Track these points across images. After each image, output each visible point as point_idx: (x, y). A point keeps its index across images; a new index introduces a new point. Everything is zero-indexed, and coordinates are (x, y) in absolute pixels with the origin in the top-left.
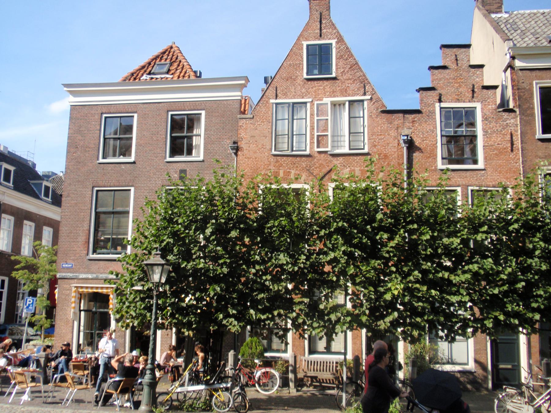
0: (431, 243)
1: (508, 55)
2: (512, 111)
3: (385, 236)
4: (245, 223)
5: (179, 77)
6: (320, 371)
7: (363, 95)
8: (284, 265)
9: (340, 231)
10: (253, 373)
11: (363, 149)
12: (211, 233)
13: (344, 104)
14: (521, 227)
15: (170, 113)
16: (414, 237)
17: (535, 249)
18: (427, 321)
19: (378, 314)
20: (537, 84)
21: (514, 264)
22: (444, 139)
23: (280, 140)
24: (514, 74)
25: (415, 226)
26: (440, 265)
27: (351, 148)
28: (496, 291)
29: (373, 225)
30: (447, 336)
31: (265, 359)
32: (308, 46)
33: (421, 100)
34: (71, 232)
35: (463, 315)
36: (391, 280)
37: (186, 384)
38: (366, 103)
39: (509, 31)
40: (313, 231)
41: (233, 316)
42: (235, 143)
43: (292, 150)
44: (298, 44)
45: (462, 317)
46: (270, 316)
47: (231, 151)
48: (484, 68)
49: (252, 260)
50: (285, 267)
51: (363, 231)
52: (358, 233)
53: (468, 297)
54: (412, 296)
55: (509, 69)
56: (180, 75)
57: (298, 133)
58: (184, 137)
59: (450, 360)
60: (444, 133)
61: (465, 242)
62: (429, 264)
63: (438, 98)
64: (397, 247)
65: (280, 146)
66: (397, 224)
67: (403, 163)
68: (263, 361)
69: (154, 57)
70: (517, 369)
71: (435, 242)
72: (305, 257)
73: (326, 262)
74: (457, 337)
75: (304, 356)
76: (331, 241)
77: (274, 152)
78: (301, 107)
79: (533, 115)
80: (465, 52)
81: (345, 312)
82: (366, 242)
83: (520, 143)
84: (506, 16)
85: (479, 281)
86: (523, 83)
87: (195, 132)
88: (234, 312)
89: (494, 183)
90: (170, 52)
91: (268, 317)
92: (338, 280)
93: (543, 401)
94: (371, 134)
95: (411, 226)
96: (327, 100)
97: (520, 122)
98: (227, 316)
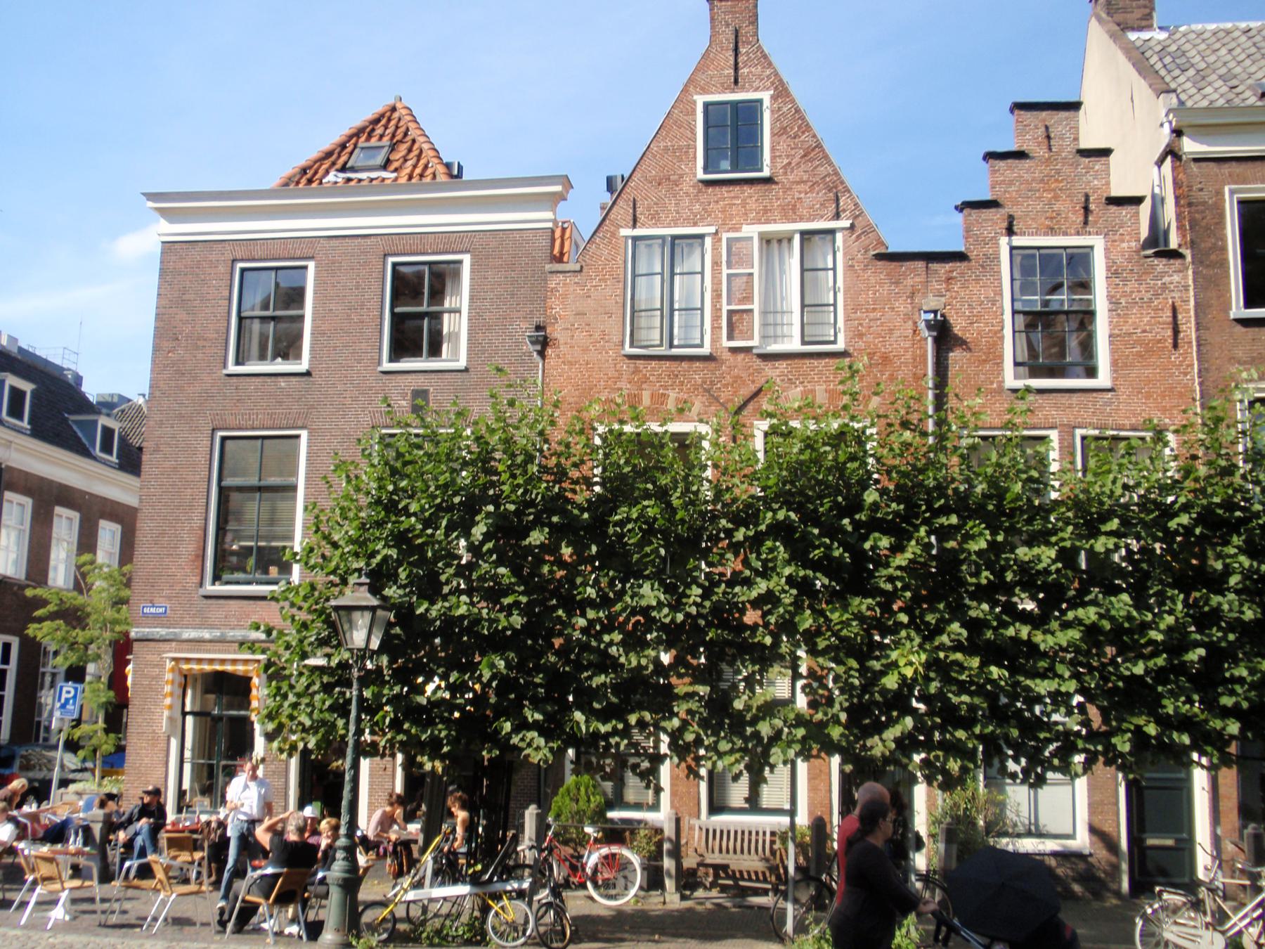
0: (989, 558)
1: (1167, 126)
2: (1175, 255)
3: (885, 542)
4: (564, 513)
5: (410, 177)
6: (735, 852)
7: (833, 219)
8: (653, 608)
9: (780, 530)
10: (582, 857)
11: (834, 342)
12: (484, 534)
13: (790, 240)
14: (1197, 522)
15: (391, 260)
16: (951, 544)
17: (1228, 571)
18: (981, 738)
19: (867, 721)
20: (1232, 192)
21: (1180, 606)
22: (1020, 319)
23: (643, 321)
24: (1181, 169)
25: (954, 519)
26: (1010, 609)
27: (806, 339)
28: (1139, 669)
29: (857, 517)
30: (1026, 771)
31: (608, 826)
32: (707, 106)
33: (968, 230)
34: (163, 534)
35: (1064, 724)
36: (897, 644)
37: (427, 881)
39: (1169, 72)
40: (719, 531)
41: (536, 726)
42: (539, 328)
43: (671, 346)
44: (683, 101)
45: (1060, 728)
47: (531, 348)
48: (1112, 157)
49: (578, 598)
50: (654, 614)
51: (833, 531)
52: (821, 535)
53: (1074, 681)
54: (947, 680)
55: (1169, 159)
56: (412, 171)
57: (683, 306)
58: (421, 316)
60: (1019, 306)
61: (1068, 557)
62: (985, 607)
63: (1005, 224)
64: (912, 568)
65: (642, 335)
66: (910, 514)
67: (925, 375)
68: (604, 830)
69: (354, 131)
70: (1186, 847)
71: (998, 557)
72: (700, 591)
73: (749, 601)
74: (1050, 775)
75: (699, 817)
76: (759, 554)
77: (628, 350)
78: (691, 245)
79: (1223, 264)
80: (1067, 118)
81: (792, 716)
82: (841, 555)
83: (1193, 330)
84: (1162, 36)
85: (1099, 646)
86: (1201, 190)
87: (447, 304)
88: (538, 716)
89: (1134, 421)
90: (389, 120)
91: (614, 728)
93: (1247, 920)
94: (852, 308)
95: (943, 520)
96: (752, 231)
97: (1194, 281)
98: (522, 725)
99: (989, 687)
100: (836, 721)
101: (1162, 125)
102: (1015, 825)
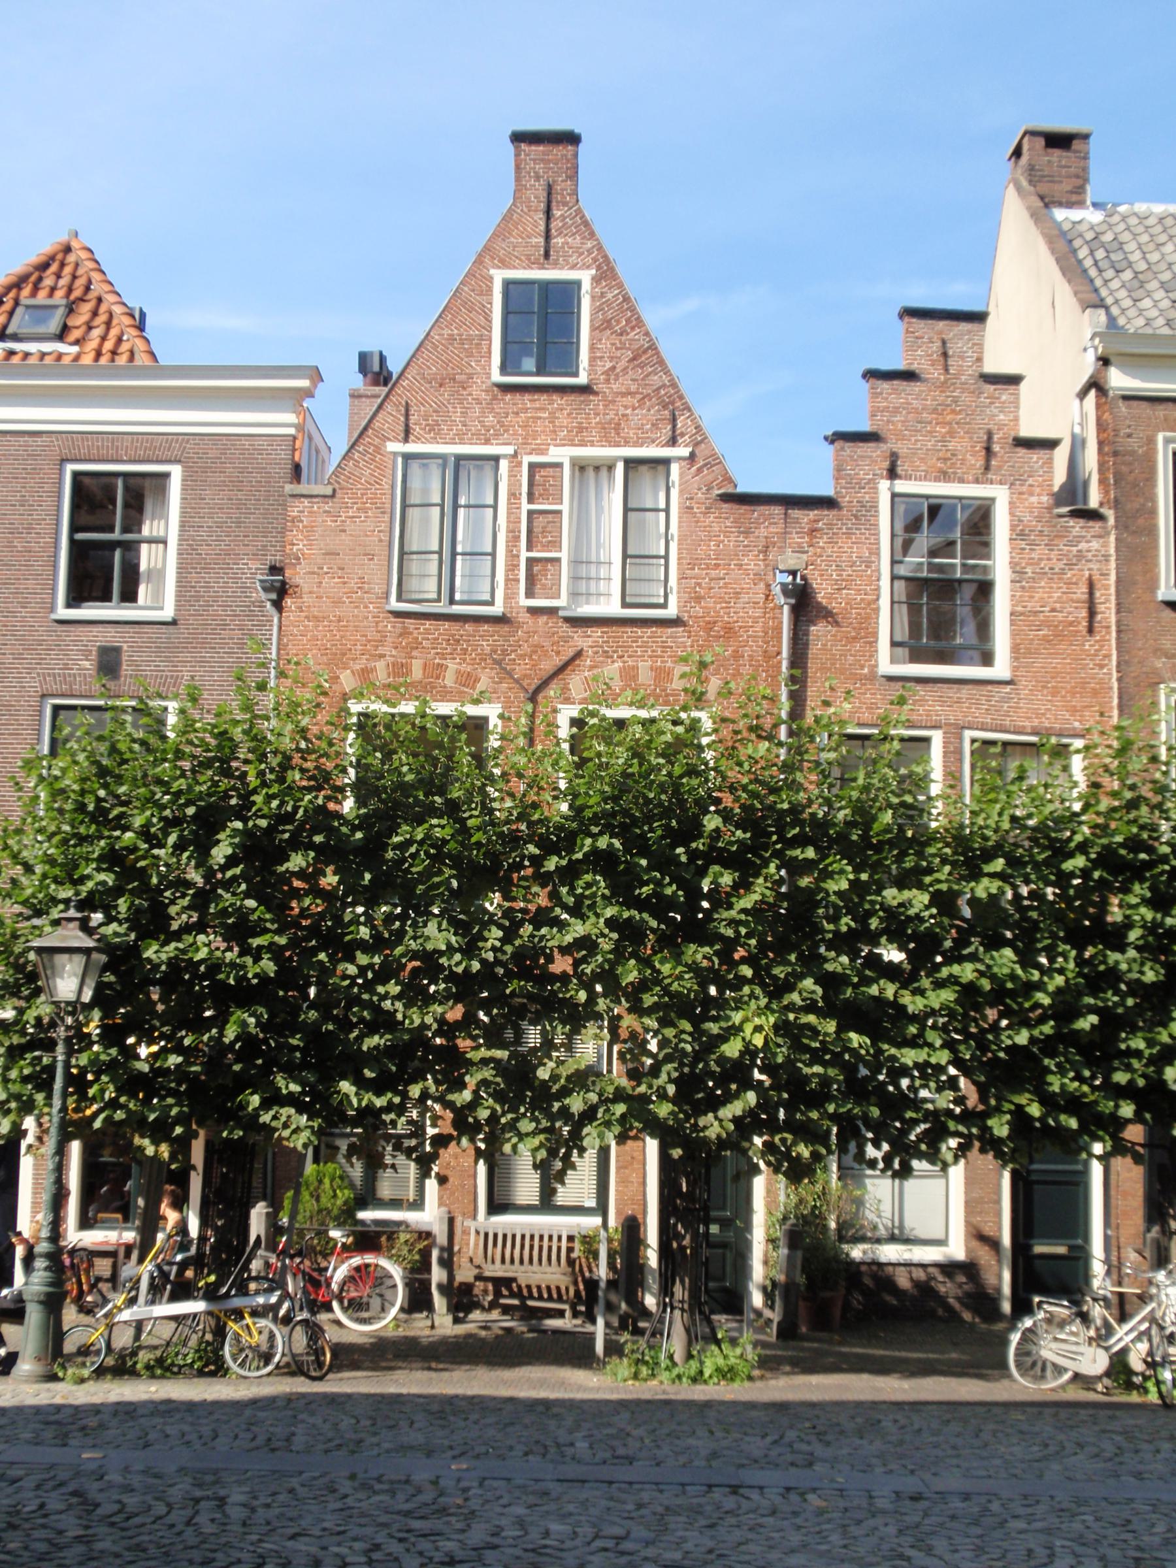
0: (851, 900)
1: (1091, 352)
2: (1093, 515)
3: (727, 879)
4: (330, 831)
5: (99, 354)
6: (522, 1262)
7: (667, 444)
8: (441, 953)
9: (602, 861)
10: (326, 1269)
11: (664, 606)
12: (227, 857)
13: (611, 468)
14: (1096, 864)
15: (70, 468)
16: (805, 882)
17: (1128, 925)
18: (835, 1118)
19: (700, 1095)
20: (1167, 441)
21: (1071, 965)
22: (900, 585)
23: (414, 566)
24: (1106, 407)
25: (810, 853)
26: (874, 961)
27: (628, 600)
28: (1022, 1038)
29: (694, 845)
30: (888, 1159)
31: (359, 1228)
32: (508, 284)
33: (839, 469)
35: (932, 1101)
36: (739, 1005)
37: (142, 1299)
38: (675, 468)
39: (1100, 271)
40: (523, 857)
41: (291, 1100)
42: (275, 569)
43: (452, 601)
44: (476, 277)
45: (930, 1106)
47: (263, 596)
48: (1023, 386)
49: (348, 938)
50: (443, 961)
51: (664, 863)
52: (650, 868)
53: (946, 1052)
54: (797, 1046)
55: (1093, 393)
56: (101, 345)
57: (468, 550)
58: (113, 545)
59: (896, 1231)
60: (902, 570)
61: (944, 902)
62: (844, 959)
63: (886, 464)
64: (755, 912)
65: (412, 584)
66: (758, 844)
67: (779, 653)
68: (353, 1233)
69: (13, 279)
70: (1079, 1257)
71: (862, 899)
72: (500, 934)
73: (560, 948)
74: (915, 1164)
75: (475, 1217)
76: (572, 889)
77: (394, 604)
78: (480, 468)
79: (1152, 531)
80: (969, 332)
81: (611, 1089)
82: (674, 893)
83: (1113, 611)
84: (1095, 217)
85: (978, 1008)
86: (1129, 436)
87: (146, 531)
88: (295, 1088)
89: (1036, 723)
90: (62, 265)
91: (390, 1102)
92: (592, 998)
93: (1134, 1334)
94: (689, 563)
95: (797, 852)
96: (561, 454)
97: (1117, 550)
98: (274, 1099)
100: (662, 1095)
101: (1085, 350)
102: (875, 1228)
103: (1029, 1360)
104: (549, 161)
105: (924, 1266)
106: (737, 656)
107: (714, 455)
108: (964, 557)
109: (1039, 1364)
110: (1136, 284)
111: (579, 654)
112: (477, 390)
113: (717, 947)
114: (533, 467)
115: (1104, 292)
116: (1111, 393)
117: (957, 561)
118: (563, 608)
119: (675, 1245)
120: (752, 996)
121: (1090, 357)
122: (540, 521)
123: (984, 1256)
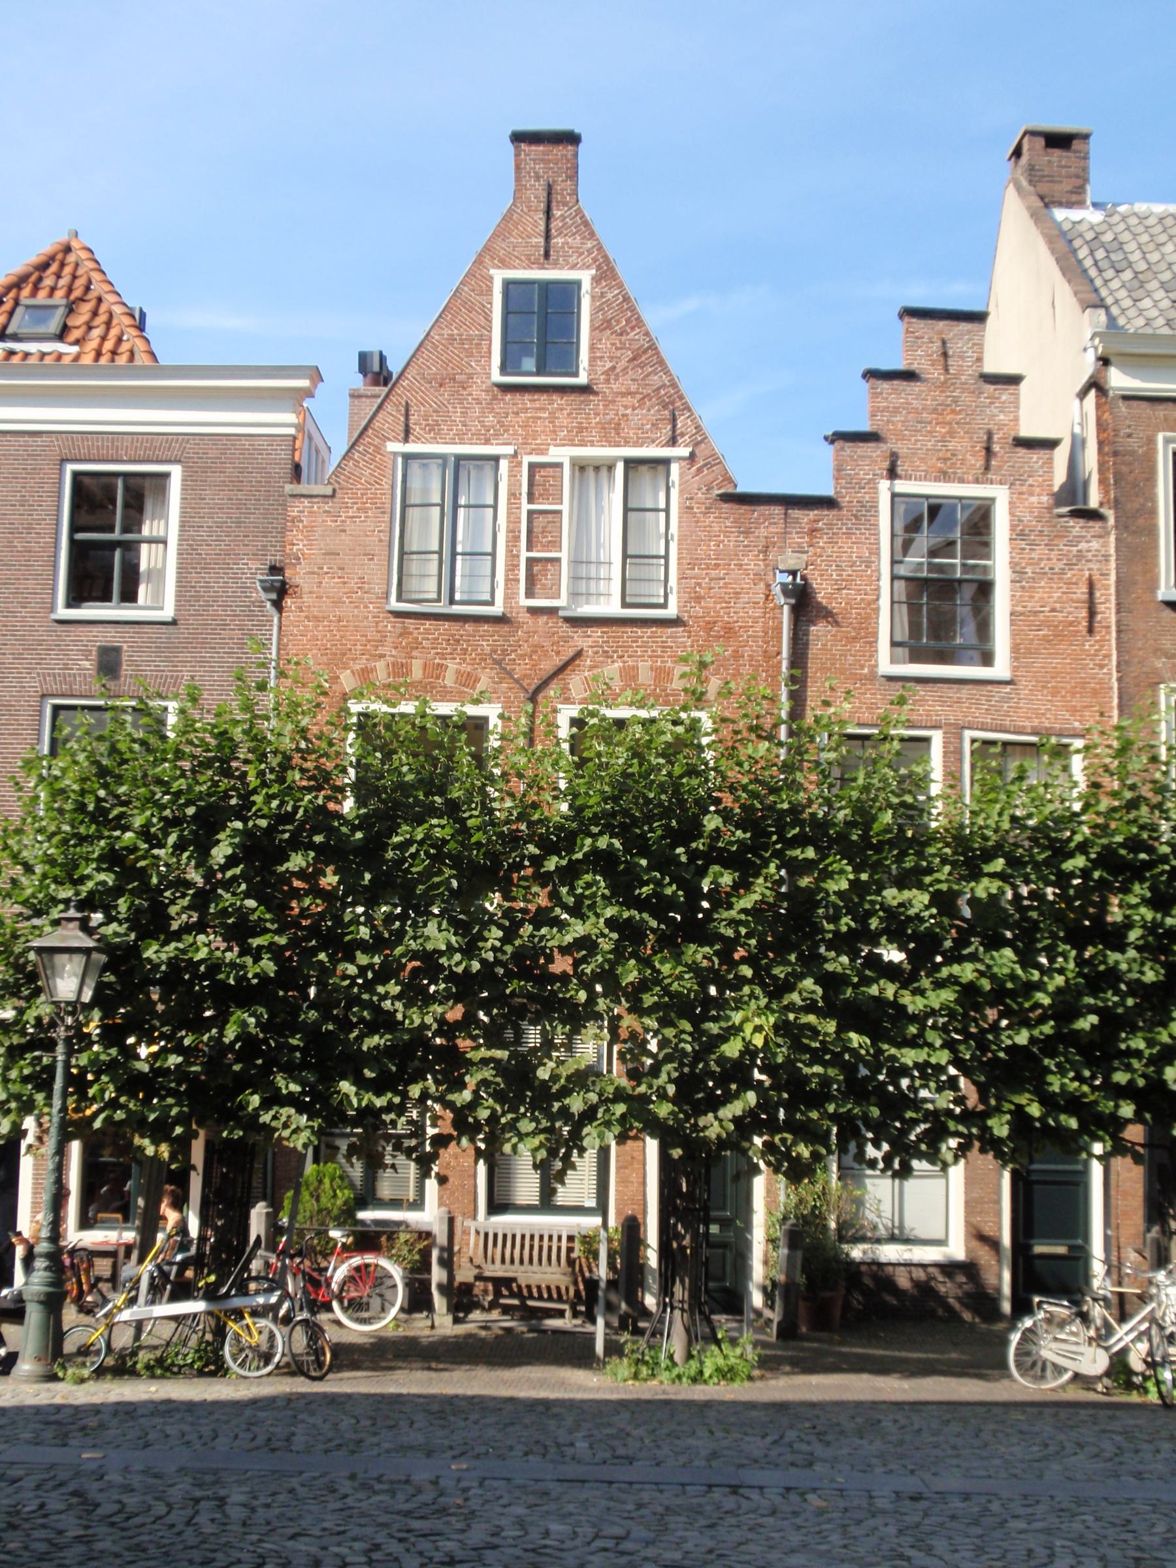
0: (851, 900)
1: (1091, 352)
2: (1093, 515)
3: (727, 879)
4: (330, 831)
5: (99, 354)
6: (522, 1262)
7: (667, 444)
8: (441, 953)
9: (602, 861)
10: (326, 1269)
11: (664, 606)
12: (227, 857)
13: (611, 468)
14: (1096, 864)
15: (70, 468)
16: (805, 882)
17: (1128, 925)
18: (835, 1118)
19: (700, 1095)
20: (1167, 441)
21: (1071, 965)
22: (900, 585)
23: (414, 566)
24: (1106, 407)
25: (810, 853)
26: (874, 961)
27: (628, 600)
28: (1022, 1038)
29: (694, 845)
30: (888, 1159)
31: (359, 1228)
32: (508, 284)
33: (839, 469)
35: (932, 1101)
36: (739, 1005)
37: (142, 1299)
38: (675, 468)
39: (1100, 271)
40: (523, 857)
41: (291, 1100)
42: (275, 569)
43: (452, 601)
44: (476, 277)
45: (930, 1106)
46: (397, 1100)
47: (263, 596)
48: (1023, 386)
49: (348, 938)
50: (443, 961)
51: (664, 863)
52: (650, 868)
53: (946, 1052)
54: (797, 1046)
55: (1093, 393)
56: (101, 345)
57: (468, 550)
58: (113, 545)
59: (896, 1231)
60: (902, 570)
61: (944, 902)
62: (844, 959)
63: (886, 464)
64: (755, 912)
65: (412, 584)
66: (758, 844)
67: (779, 653)
68: (353, 1233)
69: (13, 279)
70: (1079, 1257)
71: (862, 899)
72: (500, 934)
73: (560, 948)
74: (915, 1164)
75: (475, 1217)
76: (572, 889)
77: (394, 604)
78: (480, 468)
79: (1152, 531)
80: (969, 332)
81: (611, 1089)
82: (674, 893)
83: (1113, 611)
84: (1095, 217)
85: (978, 1008)
86: (1129, 436)
87: (146, 531)
88: (295, 1088)
89: (1036, 723)
90: (62, 265)
91: (390, 1102)
93: (1134, 1334)
94: (689, 563)
95: (797, 852)
96: (561, 454)
97: (1117, 550)
98: (274, 1099)
99: (847, 1057)
100: (662, 1095)
101: (1085, 350)
103: (1029, 1360)
104: (549, 161)
105: (924, 1266)
106: (737, 656)
107: (714, 455)
108: (964, 557)
109: (1039, 1364)
110: (1136, 284)
111: (579, 654)
112: (477, 390)
113: (717, 947)
114: (533, 467)
115: (1104, 292)
116: (1111, 393)
117: (957, 561)
118: (563, 608)
119: (675, 1245)
120: (752, 996)
121: (1090, 357)
122: (540, 521)
123: (984, 1256)
